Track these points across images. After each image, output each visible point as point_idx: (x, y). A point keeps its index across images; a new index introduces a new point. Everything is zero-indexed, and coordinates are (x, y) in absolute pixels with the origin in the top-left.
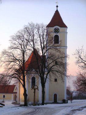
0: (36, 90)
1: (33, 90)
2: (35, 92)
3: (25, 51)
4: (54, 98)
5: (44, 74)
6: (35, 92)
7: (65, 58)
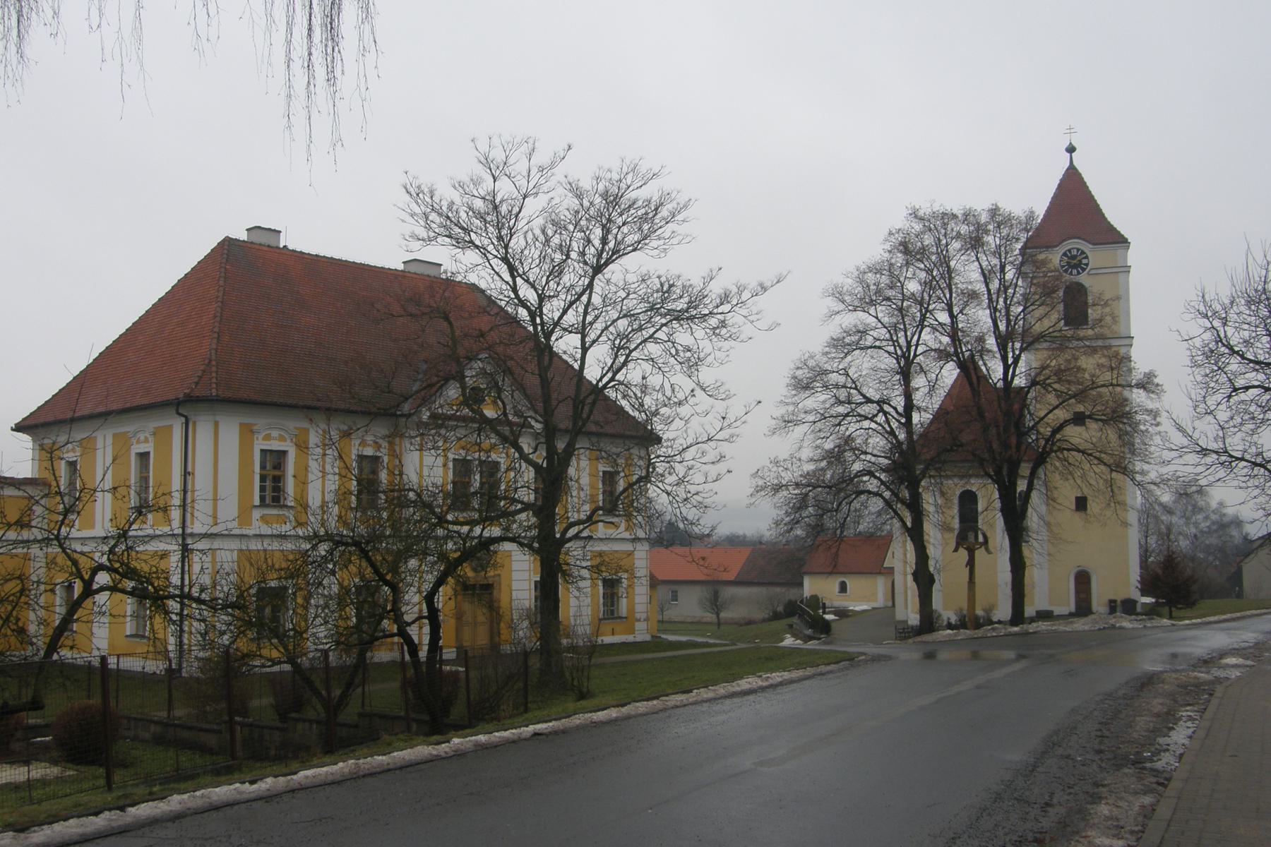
0: (980, 554)
1: (963, 554)
2: (971, 563)
3: (915, 356)
4: (1077, 592)
5: (1014, 475)
6: (971, 563)
7: (1121, 276)
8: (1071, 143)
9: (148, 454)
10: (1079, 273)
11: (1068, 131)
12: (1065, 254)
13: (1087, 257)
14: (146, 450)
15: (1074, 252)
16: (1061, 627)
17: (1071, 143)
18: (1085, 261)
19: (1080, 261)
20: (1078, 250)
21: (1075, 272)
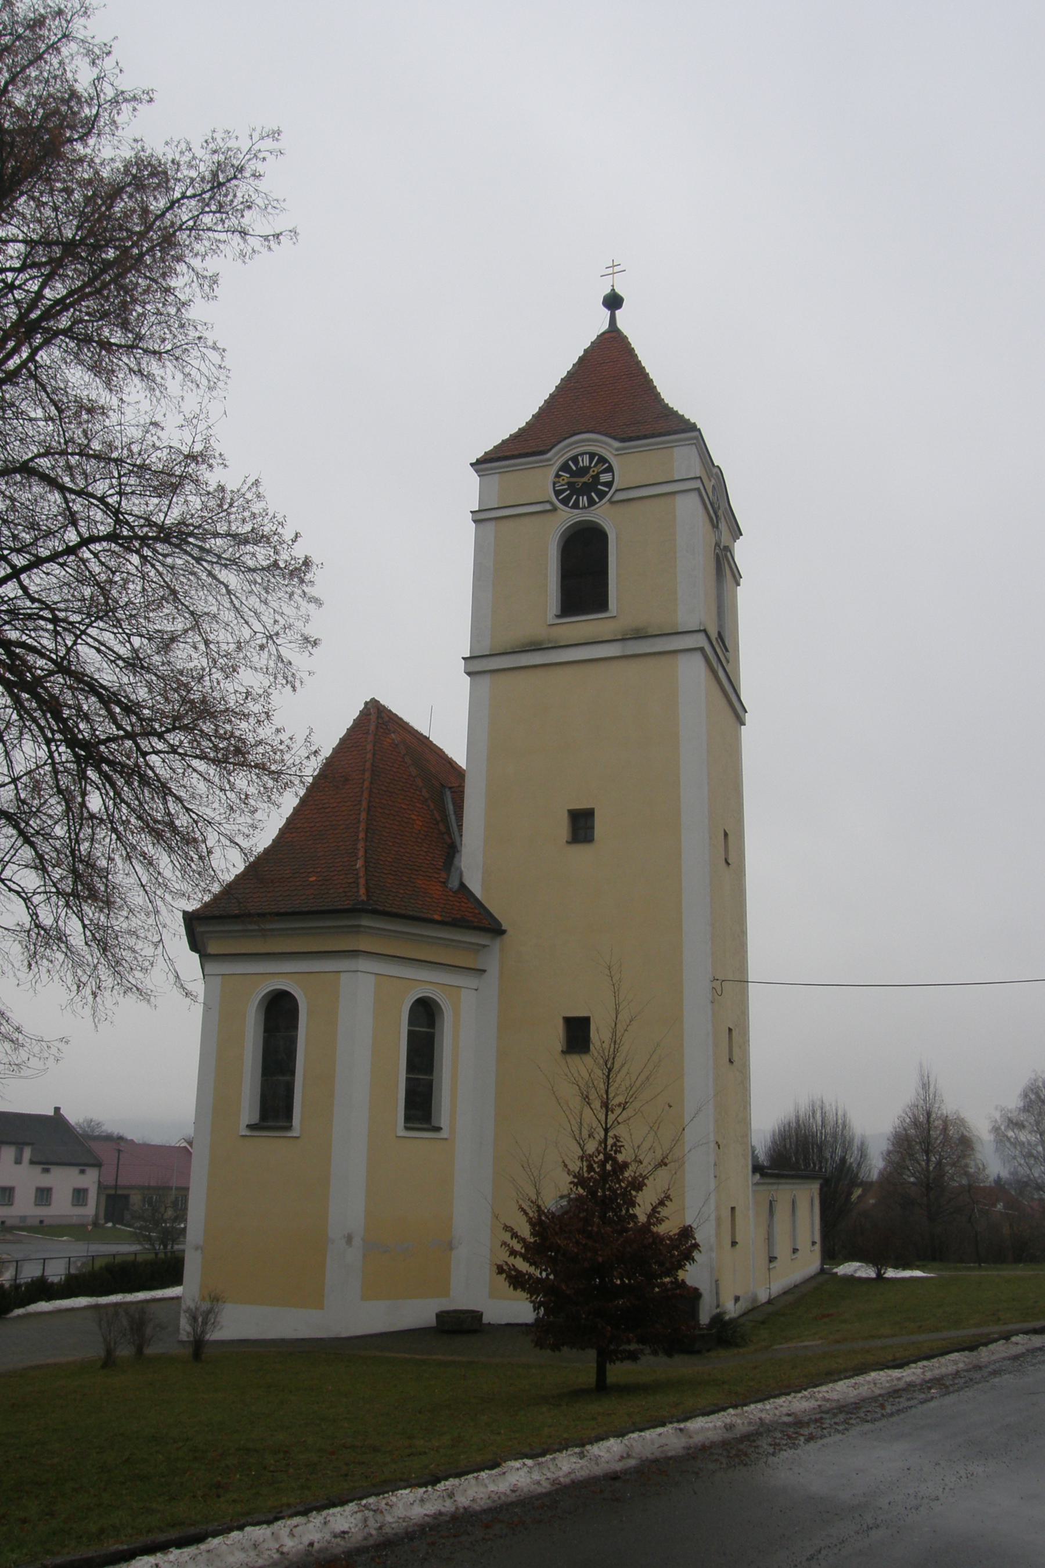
8: (613, 290)
9: (85, 1191)
10: (592, 503)
11: (610, 271)
12: (565, 467)
13: (610, 469)
14: (85, 1186)
15: (585, 461)
16: (1017, 1326)
17: (613, 290)
18: (605, 478)
19: (596, 478)
20: (592, 456)
21: (584, 500)
